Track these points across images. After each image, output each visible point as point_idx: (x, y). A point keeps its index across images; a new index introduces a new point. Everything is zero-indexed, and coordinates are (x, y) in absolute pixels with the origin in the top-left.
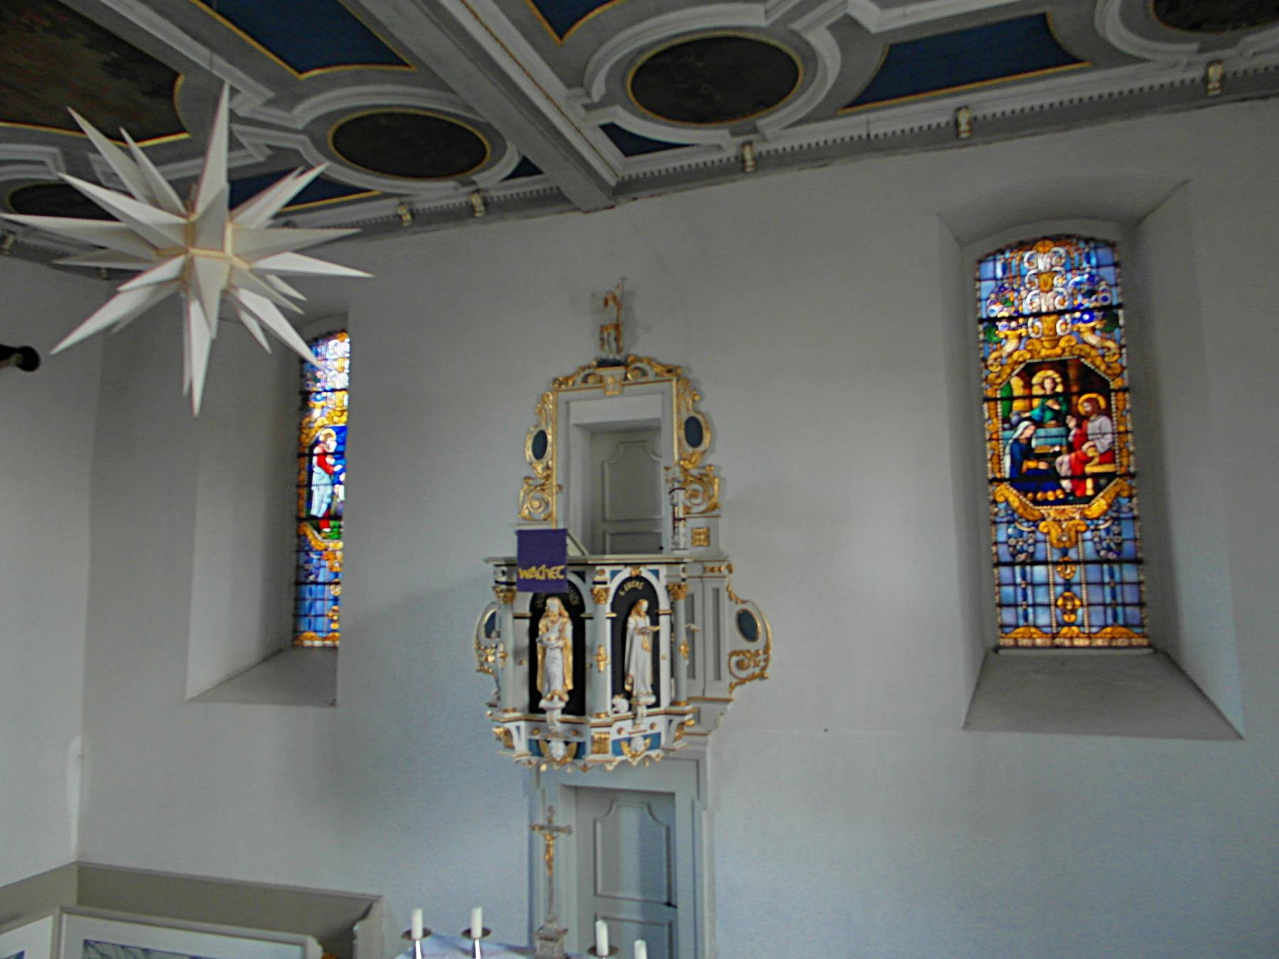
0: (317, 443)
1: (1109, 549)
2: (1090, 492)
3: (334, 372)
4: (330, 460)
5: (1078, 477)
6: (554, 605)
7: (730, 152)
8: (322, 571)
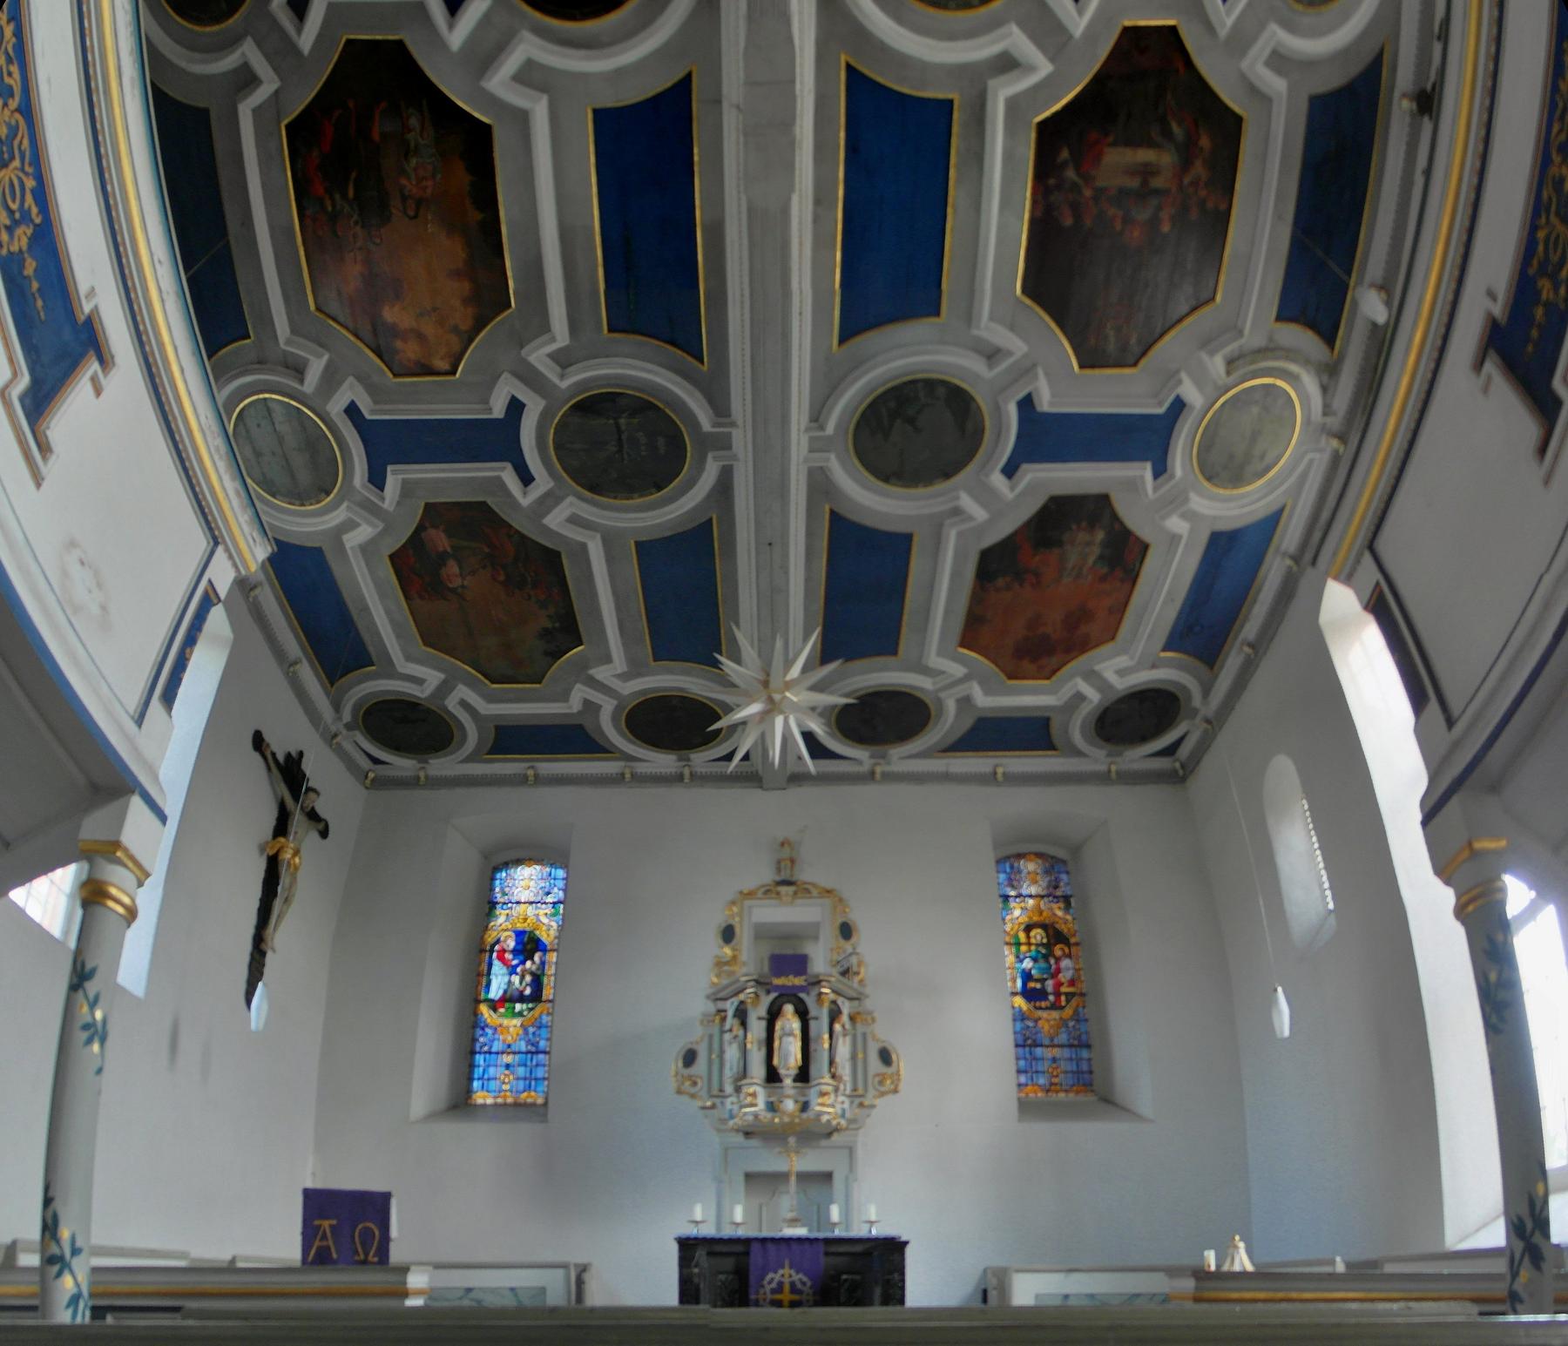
0: (498, 941)
1: (1074, 1039)
2: (1063, 1004)
3: (519, 889)
4: (508, 956)
5: (1058, 994)
6: (789, 1009)
7: (865, 768)
8: (496, 1043)
